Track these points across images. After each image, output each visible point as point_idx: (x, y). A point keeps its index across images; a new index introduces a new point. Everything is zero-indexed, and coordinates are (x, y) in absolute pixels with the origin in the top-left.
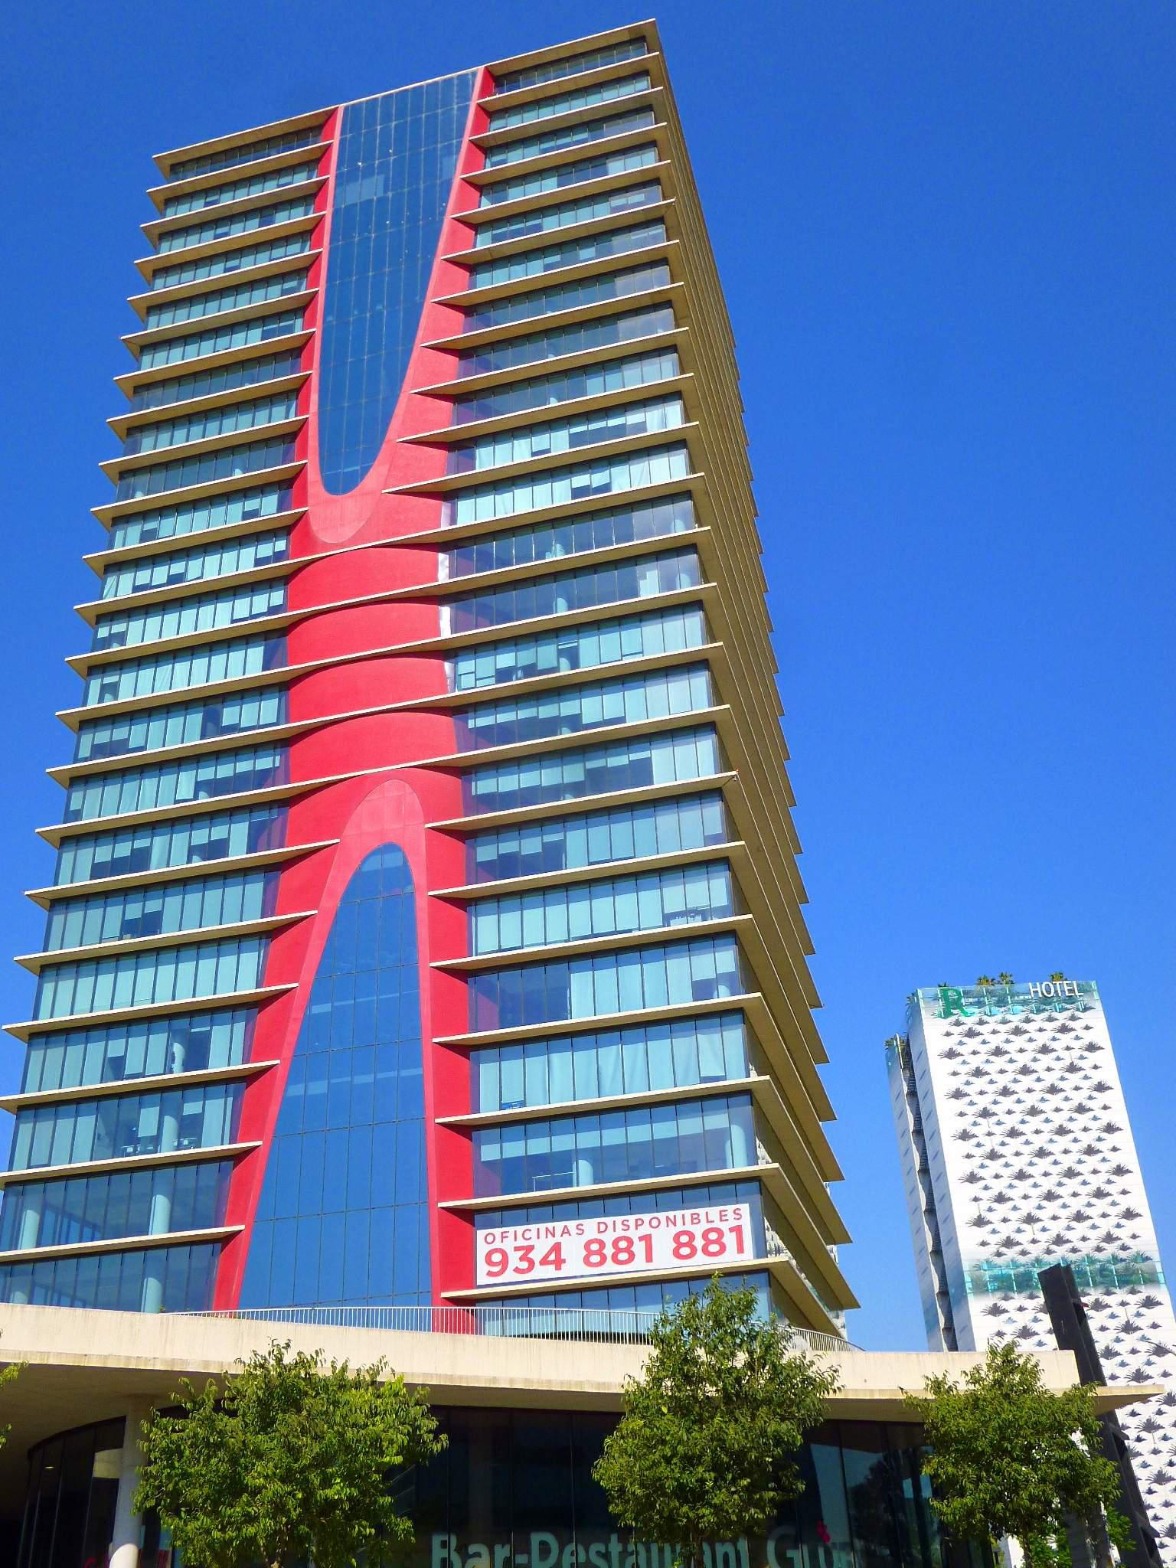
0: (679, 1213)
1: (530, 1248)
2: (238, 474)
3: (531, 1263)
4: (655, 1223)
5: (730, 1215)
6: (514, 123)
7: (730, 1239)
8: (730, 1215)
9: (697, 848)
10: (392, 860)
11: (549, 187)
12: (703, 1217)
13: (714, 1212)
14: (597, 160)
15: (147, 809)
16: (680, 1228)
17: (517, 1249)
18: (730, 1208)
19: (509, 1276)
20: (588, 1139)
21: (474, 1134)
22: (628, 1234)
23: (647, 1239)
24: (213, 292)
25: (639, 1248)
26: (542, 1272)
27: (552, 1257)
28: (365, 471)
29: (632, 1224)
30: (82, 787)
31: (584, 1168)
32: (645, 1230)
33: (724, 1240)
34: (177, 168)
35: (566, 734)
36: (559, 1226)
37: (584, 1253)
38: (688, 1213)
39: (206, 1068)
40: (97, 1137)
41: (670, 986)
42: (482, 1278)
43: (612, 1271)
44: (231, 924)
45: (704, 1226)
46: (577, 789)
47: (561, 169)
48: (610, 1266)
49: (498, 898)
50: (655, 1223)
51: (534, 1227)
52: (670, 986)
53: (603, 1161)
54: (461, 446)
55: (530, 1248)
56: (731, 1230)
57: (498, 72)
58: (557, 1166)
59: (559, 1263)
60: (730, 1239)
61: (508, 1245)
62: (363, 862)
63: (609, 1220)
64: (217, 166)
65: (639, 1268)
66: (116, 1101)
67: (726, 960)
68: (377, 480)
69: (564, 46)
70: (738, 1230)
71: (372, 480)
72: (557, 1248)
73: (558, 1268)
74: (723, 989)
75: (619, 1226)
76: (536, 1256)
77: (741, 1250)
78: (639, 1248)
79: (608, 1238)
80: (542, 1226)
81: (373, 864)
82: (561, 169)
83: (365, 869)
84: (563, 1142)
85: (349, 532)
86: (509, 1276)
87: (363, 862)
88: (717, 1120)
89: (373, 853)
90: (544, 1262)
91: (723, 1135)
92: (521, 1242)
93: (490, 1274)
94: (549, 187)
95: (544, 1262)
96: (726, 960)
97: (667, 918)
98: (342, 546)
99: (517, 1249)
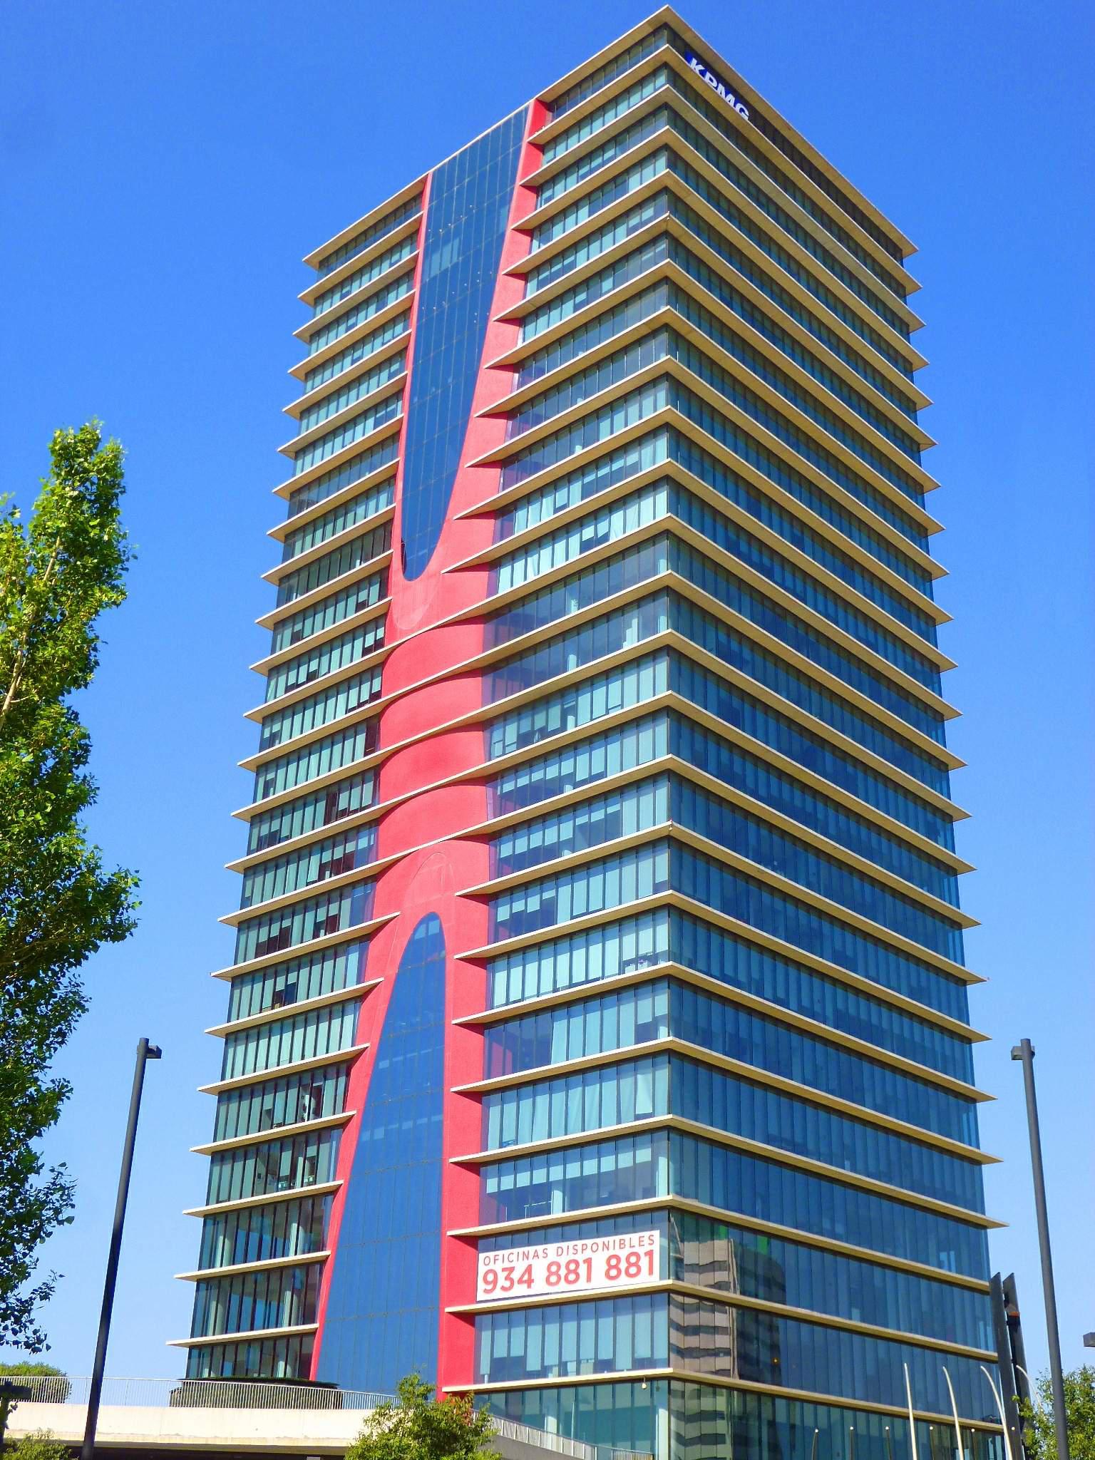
0: (611, 1239)
1: (512, 1269)
2: (579, 450)
3: (512, 1281)
4: (595, 1247)
5: (646, 1241)
6: (562, 152)
7: (644, 1262)
8: (646, 1241)
9: (648, 897)
10: (434, 927)
11: (583, 219)
12: (627, 1243)
13: (635, 1237)
14: (617, 180)
15: (291, 894)
16: (612, 1252)
17: (504, 1270)
18: (646, 1234)
19: (582, 1284)
20: (556, 1173)
21: (482, 1169)
22: (576, 1257)
23: (588, 1261)
24: (593, 233)
25: (583, 1270)
26: (520, 1290)
27: (526, 1278)
28: (431, 551)
29: (579, 1248)
30: (572, 753)
31: (557, 1196)
32: (588, 1254)
33: (579, 1271)
34: (325, 263)
35: (569, 791)
36: (531, 1249)
37: (546, 1274)
38: (617, 1238)
39: (549, 1063)
40: (257, 1176)
41: (613, 1032)
42: (481, 1296)
43: (563, 1291)
44: (630, 903)
45: (627, 1251)
46: (572, 845)
47: (590, 198)
48: (563, 1286)
49: (508, 955)
50: (595, 1247)
51: (515, 1251)
52: (613, 1032)
53: (577, 1192)
54: (502, 512)
55: (512, 1269)
56: (585, 1261)
57: (549, 99)
58: (538, 1196)
59: (530, 1282)
60: (644, 1262)
61: (498, 1267)
62: (415, 930)
63: (564, 1245)
64: (378, 234)
65: (583, 1288)
66: (581, 1076)
67: (661, 1003)
68: (441, 561)
69: (596, 57)
70: (650, 1254)
71: (433, 565)
72: (529, 1270)
73: (529, 1286)
74: (663, 1030)
75: (571, 1250)
76: (515, 1276)
77: (651, 1272)
78: (583, 1270)
79: (563, 1260)
80: (521, 1250)
81: (421, 934)
82: (590, 198)
83: (418, 936)
84: (540, 1177)
85: (417, 616)
86: (498, 1293)
87: (415, 930)
88: (644, 1155)
89: (420, 923)
90: (520, 1281)
91: (653, 1165)
92: (507, 1265)
93: (486, 1291)
94: (583, 219)
95: (520, 1281)
96: (661, 1003)
97: (623, 965)
98: (412, 631)
99: (504, 1270)
